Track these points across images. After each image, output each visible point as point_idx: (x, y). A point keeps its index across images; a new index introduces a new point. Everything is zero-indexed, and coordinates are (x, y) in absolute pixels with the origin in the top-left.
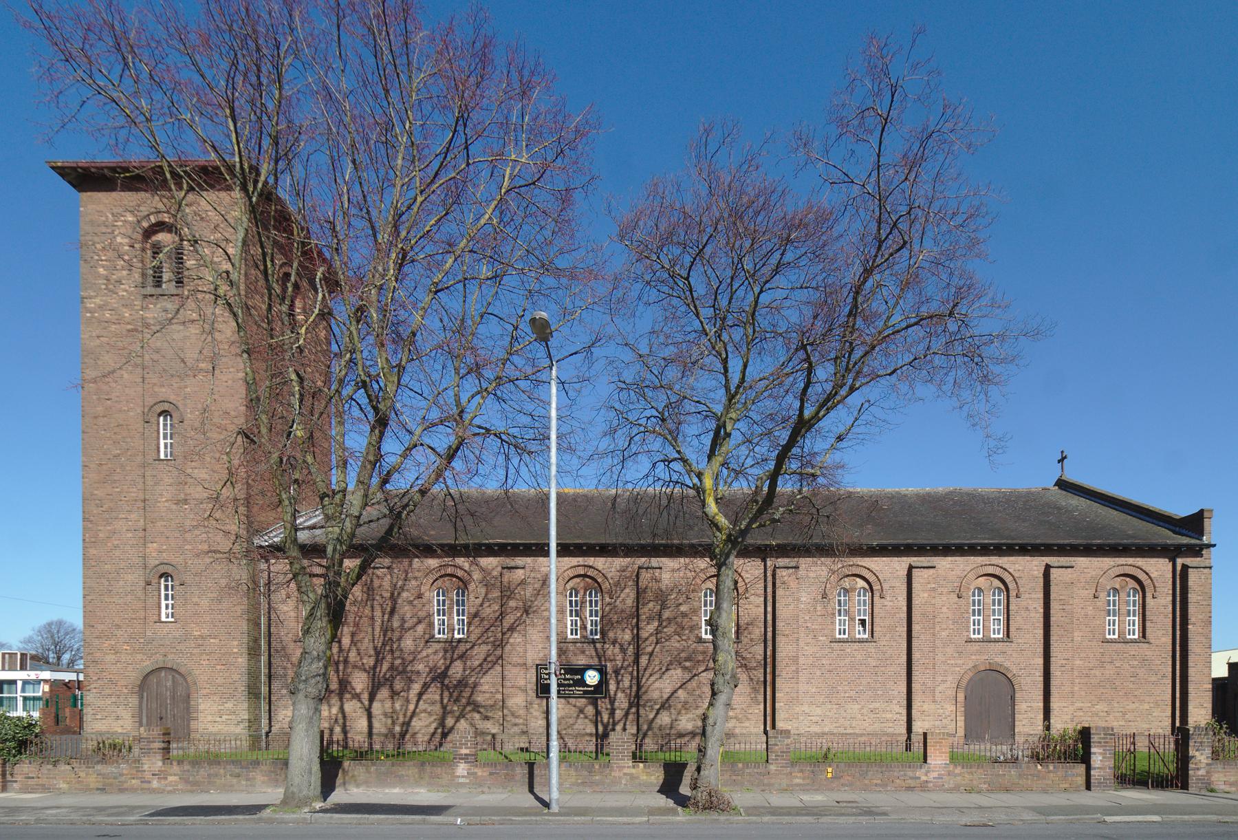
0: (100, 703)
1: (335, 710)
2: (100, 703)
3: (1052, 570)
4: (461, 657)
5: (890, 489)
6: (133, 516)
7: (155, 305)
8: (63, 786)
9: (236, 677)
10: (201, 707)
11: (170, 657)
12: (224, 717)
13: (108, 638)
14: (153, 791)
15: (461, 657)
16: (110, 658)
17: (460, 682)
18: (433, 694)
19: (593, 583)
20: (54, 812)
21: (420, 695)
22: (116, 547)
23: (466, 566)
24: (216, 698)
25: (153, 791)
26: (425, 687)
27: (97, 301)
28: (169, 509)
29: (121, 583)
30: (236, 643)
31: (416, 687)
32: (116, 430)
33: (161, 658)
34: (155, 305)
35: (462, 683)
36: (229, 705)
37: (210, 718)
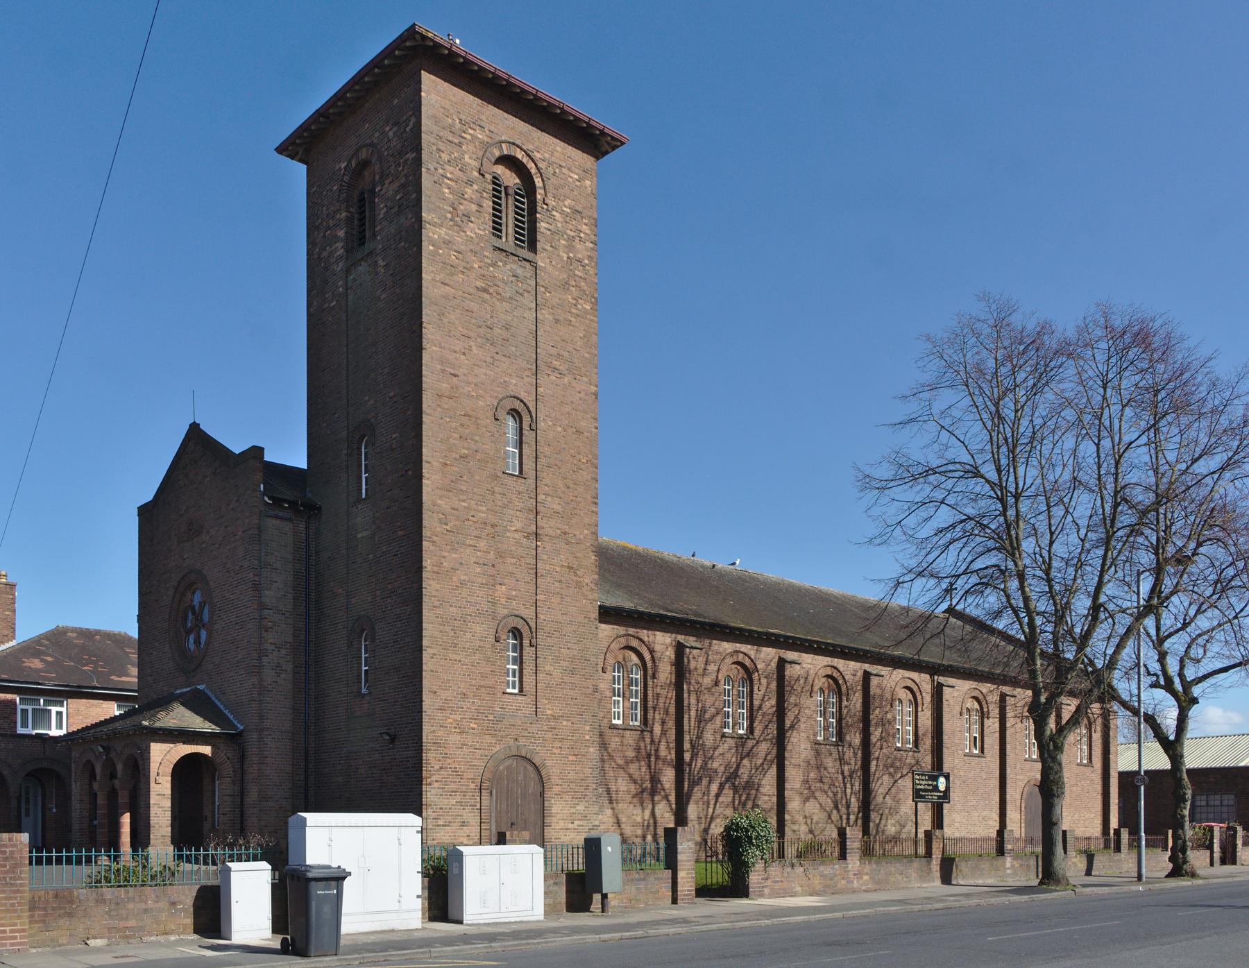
0: (443, 802)
1: (647, 813)
2: (443, 802)
3: (787, 665)
4: (748, 755)
5: (621, 542)
6: (482, 545)
7: (505, 264)
8: (799, 889)
9: (588, 771)
10: (554, 809)
11: (522, 741)
12: (576, 823)
13: (453, 712)
14: (854, 891)
15: (748, 755)
16: (455, 739)
17: (747, 782)
18: (728, 793)
19: (836, 684)
20: (800, 918)
21: (717, 796)
22: (463, 583)
23: (752, 654)
24: (567, 797)
25: (854, 891)
26: (721, 787)
27: (443, 231)
28: (518, 543)
29: (469, 635)
30: (587, 728)
31: (714, 788)
32: (465, 420)
33: (511, 742)
34: (505, 264)
35: (749, 785)
36: (581, 808)
37: (562, 824)
